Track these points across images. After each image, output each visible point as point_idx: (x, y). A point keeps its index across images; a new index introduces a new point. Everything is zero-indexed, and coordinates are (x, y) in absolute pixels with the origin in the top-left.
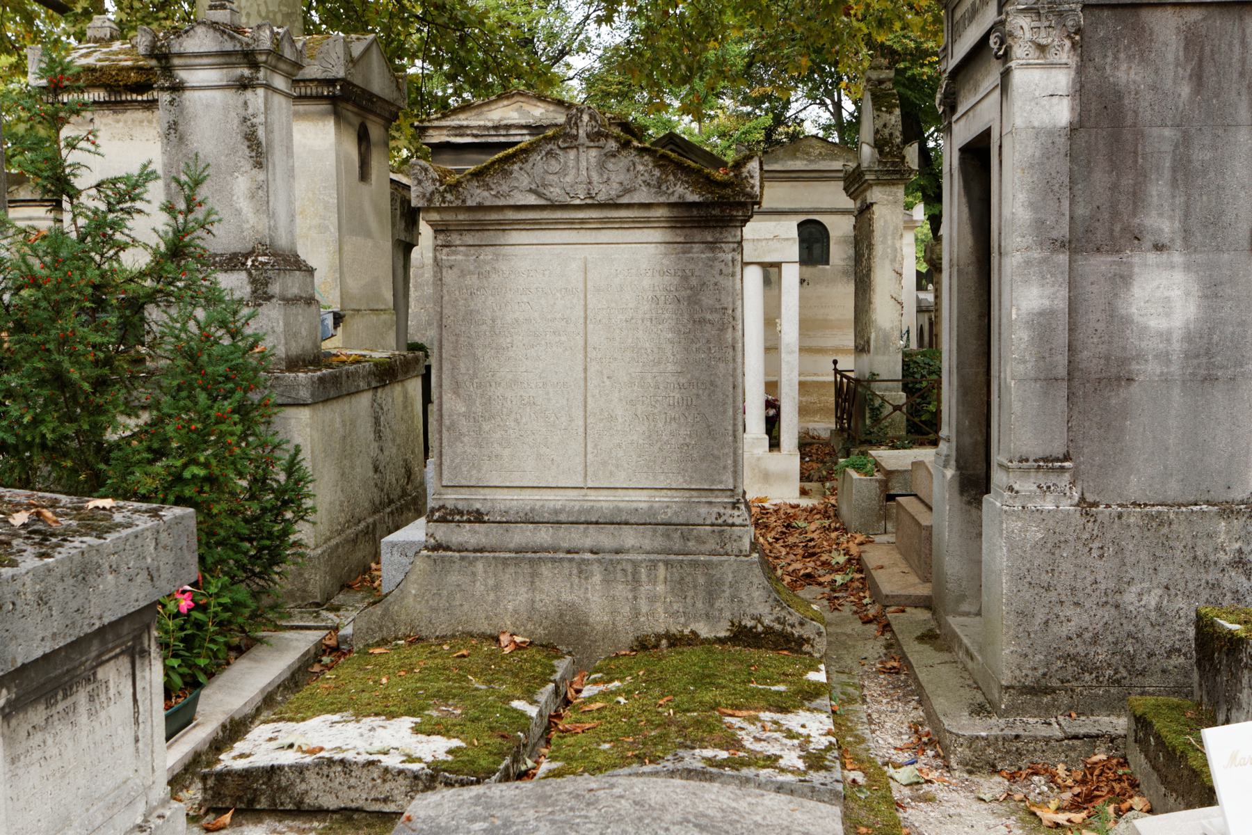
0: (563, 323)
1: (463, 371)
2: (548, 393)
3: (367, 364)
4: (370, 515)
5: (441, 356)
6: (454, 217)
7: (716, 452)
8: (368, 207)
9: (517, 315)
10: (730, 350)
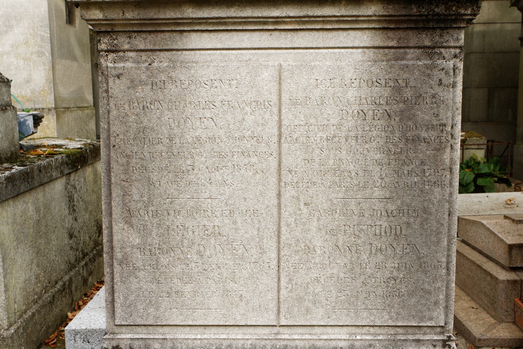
0: (254, 142)
1: (136, 197)
2: (235, 223)
3: (59, 157)
4: (66, 273)
5: (110, 180)
6: (121, 16)
7: (426, 286)
8: (73, 41)
9: (199, 132)
10: (448, 173)
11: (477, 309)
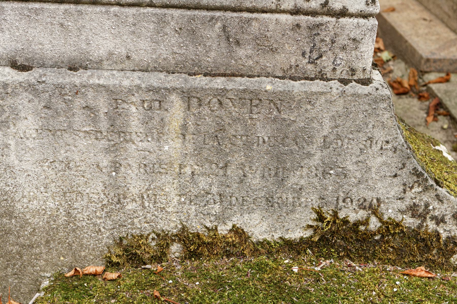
11: (431, 21)
